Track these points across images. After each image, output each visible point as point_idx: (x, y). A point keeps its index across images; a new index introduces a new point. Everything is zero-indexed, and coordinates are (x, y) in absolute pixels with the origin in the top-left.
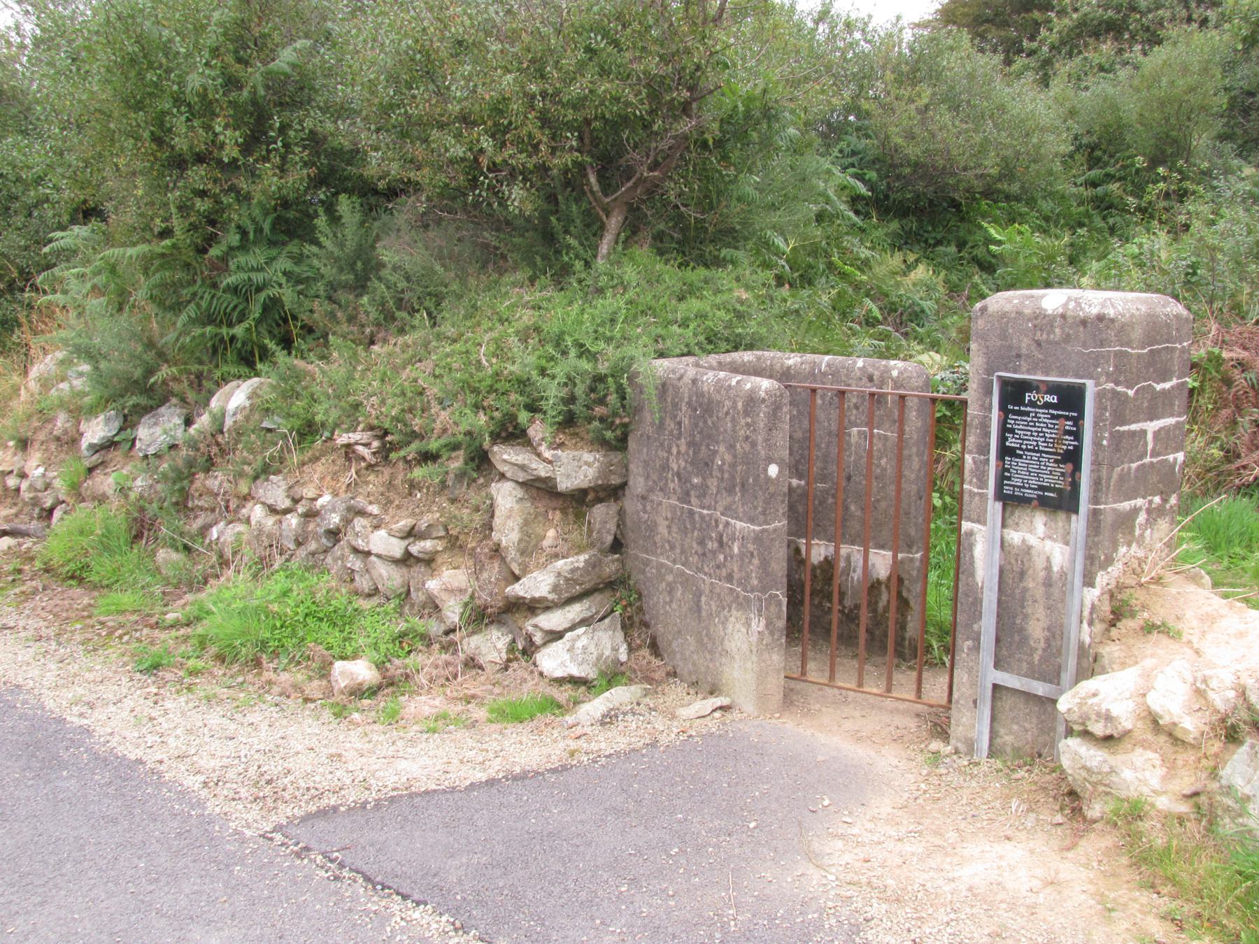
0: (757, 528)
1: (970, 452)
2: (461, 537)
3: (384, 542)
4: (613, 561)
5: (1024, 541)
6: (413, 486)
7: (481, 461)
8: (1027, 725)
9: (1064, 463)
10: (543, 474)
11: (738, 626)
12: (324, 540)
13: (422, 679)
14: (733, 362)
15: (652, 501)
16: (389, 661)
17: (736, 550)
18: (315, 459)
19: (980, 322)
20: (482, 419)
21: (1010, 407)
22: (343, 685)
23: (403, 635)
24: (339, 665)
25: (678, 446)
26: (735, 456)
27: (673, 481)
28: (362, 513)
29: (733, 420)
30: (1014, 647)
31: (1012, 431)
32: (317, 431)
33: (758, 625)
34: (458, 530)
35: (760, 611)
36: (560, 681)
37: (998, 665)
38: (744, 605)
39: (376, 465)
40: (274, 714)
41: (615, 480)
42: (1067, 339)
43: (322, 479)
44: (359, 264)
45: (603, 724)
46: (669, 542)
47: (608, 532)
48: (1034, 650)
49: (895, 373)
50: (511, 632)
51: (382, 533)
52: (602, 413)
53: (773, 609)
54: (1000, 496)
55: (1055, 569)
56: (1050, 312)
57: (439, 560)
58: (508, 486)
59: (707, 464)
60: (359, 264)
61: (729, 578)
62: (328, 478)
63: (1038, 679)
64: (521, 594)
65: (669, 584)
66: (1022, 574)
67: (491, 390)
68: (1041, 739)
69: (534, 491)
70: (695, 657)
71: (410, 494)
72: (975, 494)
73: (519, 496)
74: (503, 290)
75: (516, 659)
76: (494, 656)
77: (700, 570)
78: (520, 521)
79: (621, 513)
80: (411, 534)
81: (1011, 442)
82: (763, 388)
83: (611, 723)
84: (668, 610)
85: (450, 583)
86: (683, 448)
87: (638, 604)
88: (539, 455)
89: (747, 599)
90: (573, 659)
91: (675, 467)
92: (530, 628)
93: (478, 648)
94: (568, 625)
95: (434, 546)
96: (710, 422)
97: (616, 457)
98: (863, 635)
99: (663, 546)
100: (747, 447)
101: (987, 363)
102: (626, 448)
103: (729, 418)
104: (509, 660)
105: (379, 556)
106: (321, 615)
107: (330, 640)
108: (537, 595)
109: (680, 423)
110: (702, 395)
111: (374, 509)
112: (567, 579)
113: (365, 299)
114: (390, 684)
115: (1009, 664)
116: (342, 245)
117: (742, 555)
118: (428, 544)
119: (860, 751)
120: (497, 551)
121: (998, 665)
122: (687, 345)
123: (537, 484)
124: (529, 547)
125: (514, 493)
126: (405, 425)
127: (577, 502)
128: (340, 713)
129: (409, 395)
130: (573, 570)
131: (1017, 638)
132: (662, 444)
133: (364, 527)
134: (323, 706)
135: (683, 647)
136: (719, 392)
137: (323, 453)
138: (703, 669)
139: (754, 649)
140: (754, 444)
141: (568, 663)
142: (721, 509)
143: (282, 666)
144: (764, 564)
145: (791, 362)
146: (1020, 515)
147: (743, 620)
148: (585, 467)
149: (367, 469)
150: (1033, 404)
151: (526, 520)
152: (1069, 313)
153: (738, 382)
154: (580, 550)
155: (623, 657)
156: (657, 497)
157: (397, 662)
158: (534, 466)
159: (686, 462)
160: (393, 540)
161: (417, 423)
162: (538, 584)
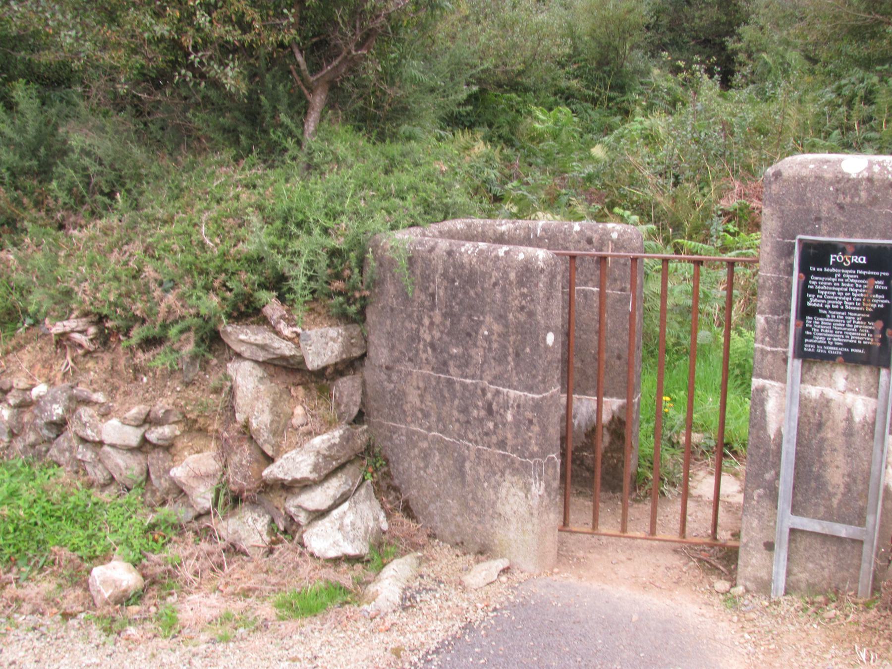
0: (536, 396)
1: (762, 313)
2: (201, 420)
3: (116, 431)
4: (363, 433)
5: (822, 394)
6: (138, 370)
7: (212, 341)
8: (823, 563)
9: (874, 321)
10: (287, 353)
11: (513, 490)
12: (45, 432)
13: (186, 572)
14: (450, 231)
15: (400, 372)
16: (145, 556)
17: (509, 417)
18: (19, 347)
19: (773, 187)
20: (215, 300)
21: (812, 269)
22: (107, 595)
23: (153, 527)
24: (98, 572)
25: (430, 317)
26: (506, 326)
27: (425, 351)
28: (87, 402)
29: (503, 290)
30: (810, 493)
31: (815, 292)
32: (18, 319)
33: (538, 489)
34: (196, 413)
35: (540, 476)
36: (336, 561)
37: (796, 509)
38: (521, 470)
39: (95, 351)
40: (36, 643)
41: (356, 353)
42: (874, 201)
43: (32, 367)
44: (42, 150)
45: (405, 608)
46: (422, 410)
47: (355, 405)
48: (831, 495)
49: (615, 236)
50: (268, 513)
51: (115, 422)
52: (349, 289)
53: (551, 471)
54: (800, 353)
55: (857, 419)
56: (854, 176)
57: (179, 445)
58: (247, 366)
59: (469, 335)
60: (42, 150)
61: (502, 444)
62: (39, 366)
63: (837, 521)
64: (281, 476)
65: (422, 450)
66: (820, 426)
67: (221, 270)
68: (839, 575)
69: (272, 368)
70: (459, 519)
71: (136, 379)
72: (767, 352)
73: (260, 375)
74: (209, 170)
75: (279, 541)
76: (256, 540)
77: (460, 437)
78: (270, 402)
79: (364, 383)
80: (148, 421)
81: (813, 302)
82: (540, 257)
83: (412, 606)
84: (422, 475)
85: (195, 467)
86: (438, 319)
87: (386, 469)
88: (278, 333)
89: (526, 466)
90: (345, 538)
91: (428, 338)
92: (293, 510)
93: (235, 532)
94: (330, 502)
95: (173, 432)
96: (472, 293)
97: (355, 330)
98: (598, 480)
99: (414, 414)
100: (522, 317)
101: (782, 227)
102: (364, 320)
103: (497, 289)
104: (273, 543)
105: (113, 446)
106: (59, 514)
107: (76, 541)
108: (298, 476)
109: (433, 295)
110: (462, 266)
111: (100, 397)
112: (325, 457)
113: (54, 184)
114: (157, 583)
115: (804, 509)
116: (22, 130)
117: (517, 423)
118: (166, 431)
119: (655, 601)
120: (247, 433)
121: (796, 509)
122: (412, 217)
123: (276, 362)
124: (282, 427)
125: (255, 372)
126: (124, 309)
127: (320, 380)
128: (111, 627)
129: (124, 278)
130: (330, 447)
131: (813, 484)
132: (410, 316)
133: (92, 416)
134: (86, 620)
135: (446, 509)
136: (483, 263)
137: (28, 341)
138: (469, 531)
139: (535, 512)
140: (531, 314)
141: (341, 543)
142: (489, 378)
143: (24, 576)
144: (544, 429)
145: (503, 228)
146: (821, 371)
147: (521, 484)
148: (331, 343)
149: (85, 355)
150: (837, 265)
151: (274, 400)
152: (876, 177)
153: (506, 253)
154: (330, 425)
155: (385, 526)
156: (405, 367)
157: (154, 557)
158: (276, 345)
159: (442, 332)
160: (128, 429)
161: (138, 308)
162: (296, 463)
